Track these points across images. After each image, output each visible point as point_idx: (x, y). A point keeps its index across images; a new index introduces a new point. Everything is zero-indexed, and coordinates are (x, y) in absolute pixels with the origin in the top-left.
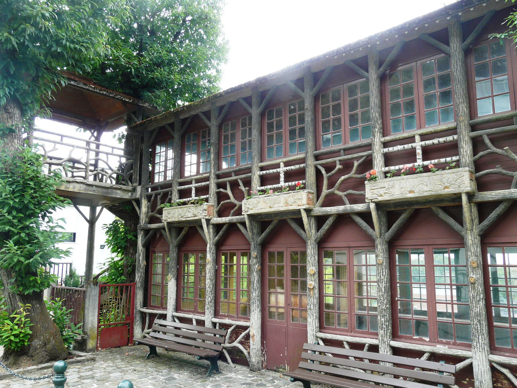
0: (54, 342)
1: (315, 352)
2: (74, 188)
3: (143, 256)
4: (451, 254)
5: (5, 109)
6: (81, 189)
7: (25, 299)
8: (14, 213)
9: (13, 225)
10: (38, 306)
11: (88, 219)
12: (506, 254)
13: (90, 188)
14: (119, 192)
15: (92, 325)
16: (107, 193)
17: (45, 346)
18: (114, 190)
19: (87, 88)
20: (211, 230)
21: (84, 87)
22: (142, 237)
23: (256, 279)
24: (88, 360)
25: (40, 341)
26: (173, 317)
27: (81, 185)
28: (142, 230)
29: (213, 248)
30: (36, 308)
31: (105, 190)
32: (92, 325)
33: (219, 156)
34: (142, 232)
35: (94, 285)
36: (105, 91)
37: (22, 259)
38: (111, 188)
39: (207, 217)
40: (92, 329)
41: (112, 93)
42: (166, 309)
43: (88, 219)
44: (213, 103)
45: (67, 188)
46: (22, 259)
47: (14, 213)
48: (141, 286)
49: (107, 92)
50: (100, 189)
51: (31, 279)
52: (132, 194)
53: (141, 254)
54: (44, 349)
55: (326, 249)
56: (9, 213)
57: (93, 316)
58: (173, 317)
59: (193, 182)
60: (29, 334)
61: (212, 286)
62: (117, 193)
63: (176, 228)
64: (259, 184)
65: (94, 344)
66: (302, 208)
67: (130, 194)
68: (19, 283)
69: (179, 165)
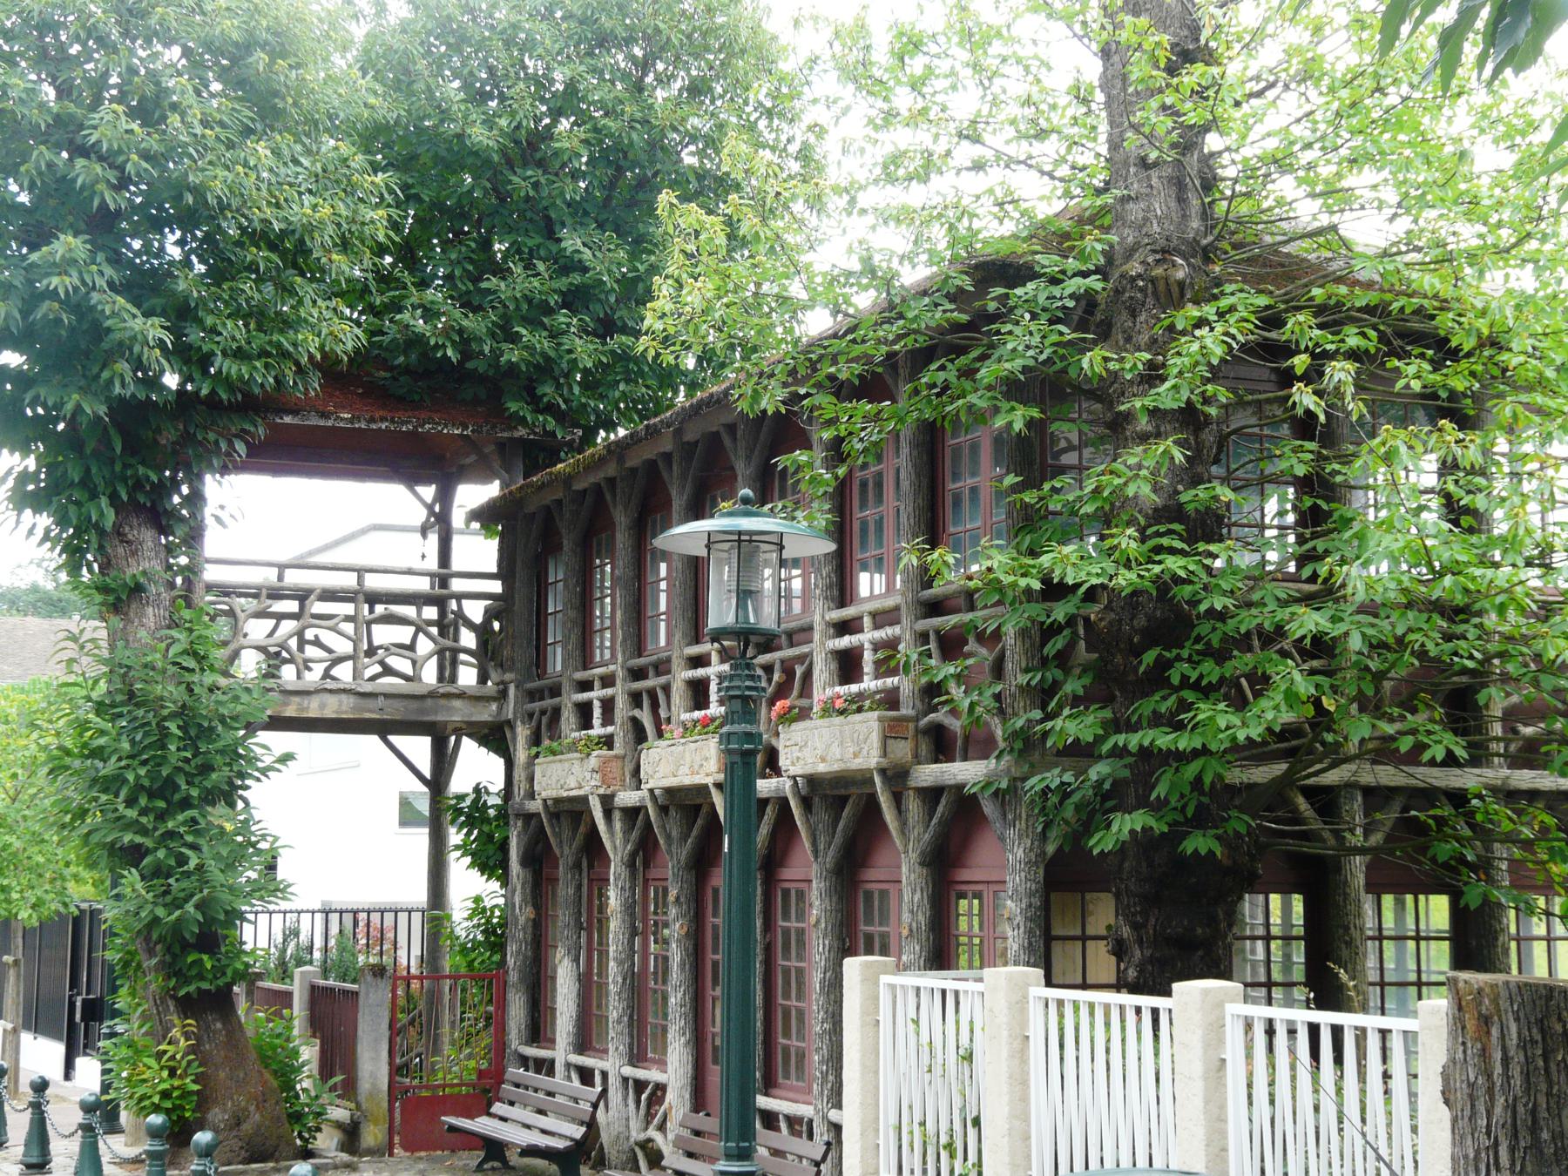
0: (257, 1117)
1: (801, 1158)
2: (322, 706)
3: (523, 893)
4: (1272, 896)
5: (119, 534)
6: (344, 708)
7: (188, 1006)
8: (143, 801)
9: (144, 831)
10: (219, 1025)
11: (428, 776)
12: (1422, 897)
13: (370, 703)
14: (457, 703)
15: (374, 1085)
16: (422, 711)
17: (238, 1125)
18: (443, 702)
19: (330, 423)
20: (618, 825)
21: (322, 423)
22: (518, 836)
23: (677, 959)
24: (336, 1167)
25: (225, 1111)
26: (568, 1065)
27: (344, 697)
28: (517, 816)
29: (624, 873)
30: (214, 1032)
31: (414, 705)
32: (374, 1085)
33: (639, 613)
34: (520, 823)
35: (375, 975)
36: (382, 419)
37: (160, 912)
38: (432, 695)
39: (601, 791)
40: (372, 1095)
41: (407, 423)
42: (551, 1043)
43: (428, 776)
44: (621, 460)
45: (303, 710)
46: (160, 912)
47: (143, 801)
48: (521, 980)
49: (393, 421)
50: (397, 704)
51: (190, 960)
52: (500, 709)
53: (519, 887)
54: (234, 1133)
55: (786, 885)
56: (130, 803)
57: (375, 1059)
58: (568, 1065)
59: (597, 684)
60: (192, 1093)
61: (620, 980)
62: (449, 709)
63: (570, 812)
64: (691, 703)
65: (380, 1136)
66: (709, 781)
67: (494, 707)
68: (173, 970)
69: (577, 631)
